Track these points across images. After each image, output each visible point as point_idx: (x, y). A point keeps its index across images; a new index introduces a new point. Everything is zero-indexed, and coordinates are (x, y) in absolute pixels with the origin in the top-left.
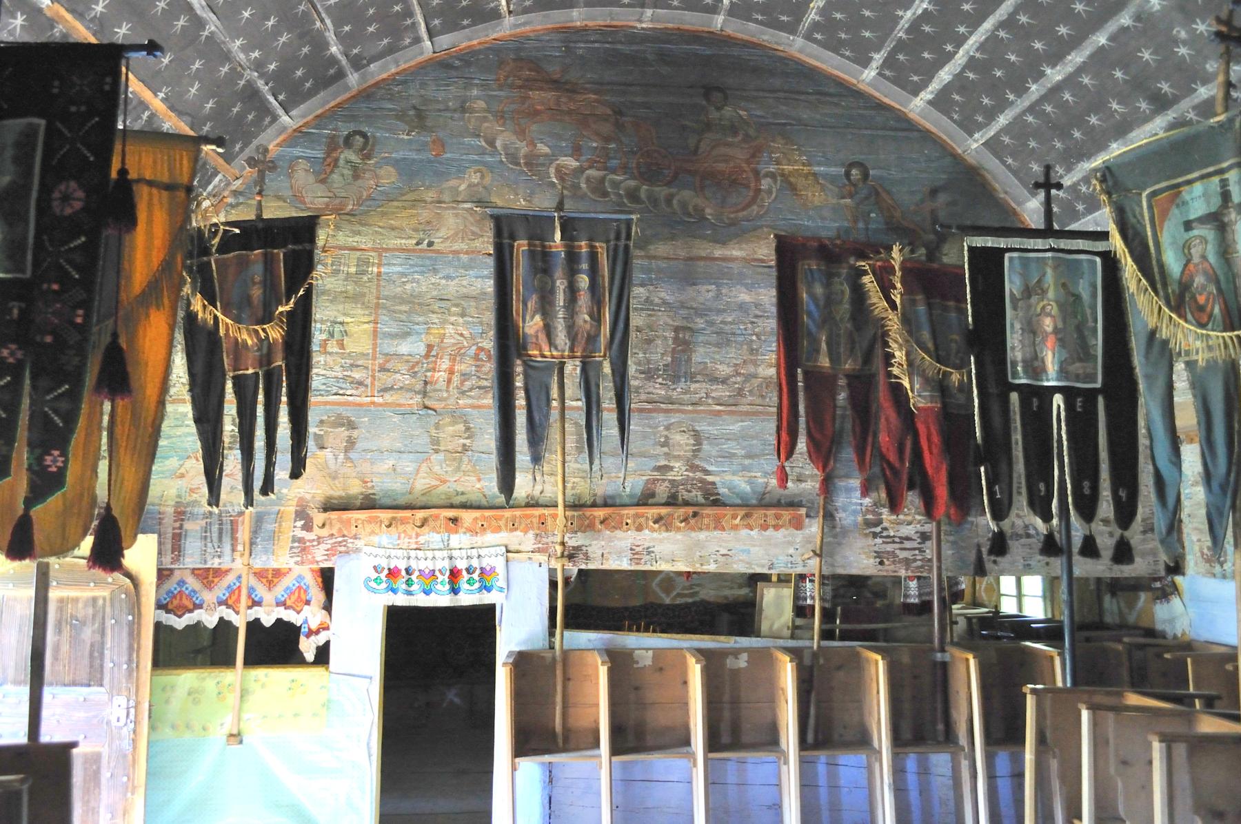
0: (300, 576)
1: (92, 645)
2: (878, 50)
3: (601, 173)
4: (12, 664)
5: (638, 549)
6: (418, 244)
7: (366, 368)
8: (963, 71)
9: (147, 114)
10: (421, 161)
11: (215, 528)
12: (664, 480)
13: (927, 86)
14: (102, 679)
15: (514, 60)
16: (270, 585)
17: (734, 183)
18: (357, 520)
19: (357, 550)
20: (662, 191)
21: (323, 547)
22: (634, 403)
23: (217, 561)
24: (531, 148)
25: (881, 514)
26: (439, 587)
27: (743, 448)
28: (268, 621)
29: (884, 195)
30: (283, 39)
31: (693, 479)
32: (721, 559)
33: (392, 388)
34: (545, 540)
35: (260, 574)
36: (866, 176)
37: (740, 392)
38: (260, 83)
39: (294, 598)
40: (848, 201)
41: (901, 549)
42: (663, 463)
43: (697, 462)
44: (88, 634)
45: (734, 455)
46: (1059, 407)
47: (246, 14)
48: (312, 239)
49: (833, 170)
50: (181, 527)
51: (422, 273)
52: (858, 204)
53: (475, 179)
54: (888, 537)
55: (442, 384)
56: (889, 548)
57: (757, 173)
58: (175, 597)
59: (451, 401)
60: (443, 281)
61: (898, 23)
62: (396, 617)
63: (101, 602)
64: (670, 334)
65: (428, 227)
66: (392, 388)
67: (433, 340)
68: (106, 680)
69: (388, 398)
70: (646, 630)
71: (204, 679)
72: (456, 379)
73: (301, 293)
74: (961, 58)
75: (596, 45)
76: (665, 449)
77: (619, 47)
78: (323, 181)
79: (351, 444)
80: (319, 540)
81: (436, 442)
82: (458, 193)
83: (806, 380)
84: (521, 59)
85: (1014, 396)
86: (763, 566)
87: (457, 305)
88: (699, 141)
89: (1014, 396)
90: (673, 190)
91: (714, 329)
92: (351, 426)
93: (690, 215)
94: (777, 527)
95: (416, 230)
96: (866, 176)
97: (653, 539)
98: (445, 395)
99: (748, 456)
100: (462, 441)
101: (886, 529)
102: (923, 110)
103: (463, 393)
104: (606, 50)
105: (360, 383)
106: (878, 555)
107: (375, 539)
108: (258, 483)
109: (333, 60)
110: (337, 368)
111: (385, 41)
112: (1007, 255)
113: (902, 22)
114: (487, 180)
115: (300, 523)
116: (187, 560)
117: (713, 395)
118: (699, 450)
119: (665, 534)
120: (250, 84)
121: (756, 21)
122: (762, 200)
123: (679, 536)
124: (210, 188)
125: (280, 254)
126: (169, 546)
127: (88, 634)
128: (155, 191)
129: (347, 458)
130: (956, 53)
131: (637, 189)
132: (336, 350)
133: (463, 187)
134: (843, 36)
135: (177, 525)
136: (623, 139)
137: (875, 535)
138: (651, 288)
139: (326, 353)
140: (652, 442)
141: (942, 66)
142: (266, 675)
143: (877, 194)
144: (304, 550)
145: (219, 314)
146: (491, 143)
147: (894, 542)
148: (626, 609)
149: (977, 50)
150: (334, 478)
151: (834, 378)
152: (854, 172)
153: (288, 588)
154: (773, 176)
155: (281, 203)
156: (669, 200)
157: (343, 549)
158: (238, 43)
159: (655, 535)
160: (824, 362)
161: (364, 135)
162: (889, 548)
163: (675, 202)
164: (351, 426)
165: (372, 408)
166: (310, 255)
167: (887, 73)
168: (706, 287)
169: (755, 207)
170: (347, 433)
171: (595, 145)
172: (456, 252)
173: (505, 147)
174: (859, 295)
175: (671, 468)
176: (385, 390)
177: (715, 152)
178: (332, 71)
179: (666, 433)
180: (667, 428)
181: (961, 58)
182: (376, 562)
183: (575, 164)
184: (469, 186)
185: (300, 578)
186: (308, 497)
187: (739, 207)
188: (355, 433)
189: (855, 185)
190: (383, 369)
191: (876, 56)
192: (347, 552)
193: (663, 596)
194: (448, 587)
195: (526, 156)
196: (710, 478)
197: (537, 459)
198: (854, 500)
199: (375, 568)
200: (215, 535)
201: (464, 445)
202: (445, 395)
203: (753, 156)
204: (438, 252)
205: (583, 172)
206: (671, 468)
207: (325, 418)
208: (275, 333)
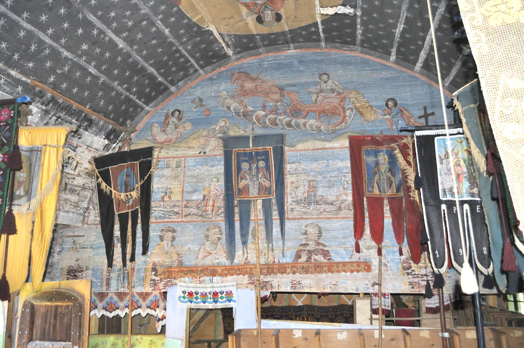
0: (155, 295)
1: (67, 325)
2: (392, 48)
3: (275, 116)
4: (39, 332)
5: (294, 282)
6: (200, 153)
7: (179, 207)
9: (83, 114)
10: (201, 119)
11: (122, 276)
12: (305, 250)
13: (418, 61)
14: (70, 339)
15: (238, 73)
16: (144, 299)
17: (334, 114)
18: (174, 271)
19: (176, 284)
20: (301, 121)
21: (162, 283)
22: (288, 214)
23: (122, 289)
24: (245, 108)
25: (410, 263)
26: (209, 300)
27: (341, 234)
28: (144, 314)
29: (405, 112)
30: (136, 79)
31: (318, 249)
32: (333, 286)
33: (190, 214)
34: (253, 279)
35: (140, 294)
36: (396, 104)
37: (340, 209)
38: (132, 96)
39: (154, 305)
40: (388, 116)
41: (422, 280)
42: (304, 242)
43: (320, 241)
44: (66, 320)
45: (338, 237)
47: (116, 72)
48: (151, 155)
49: (379, 104)
50: (109, 275)
51: (202, 165)
52: (393, 118)
53: (223, 124)
54: (415, 274)
55: (210, 212)
56: (416, 280)
57: (344, 109)
58: (109, 304)
59: (214, 219)
60: (210, 168)
61: (395, 35)
62: (192, 312)
63: (70, 307)
64: (307, 184)
65: (204, 146)
66: (190, 214)
67: (206, 193)
68: (71, 340)
69: (189, 218)
70: (296, 320)
71: (118, 339)
72: (215, 209)
73: (146, 178)
75: (272, 62)
76: (305, 236)
77: (281, 61)
78: (164, 131)
79: (174, 238)
80: (161, 280)
81: (207, 237)
82: (216, 131)
83: (368, 201)
84: (241, 72)
85: (444, 207)
86: (353, 290)
87: (216, 177)
88: (317, 97)
90: (307, 120)
91: (326, 180)
92: (174, 231)
93: (314, 131)
94: (358, 271)
95: (199, 147)
96: (396, 104)
97: (301, 278)
98: (211, 216)
99: (344, 237)
100: (218, 236)
101: (414, 271)
102: (420, 71)
103: (218, 215)
104: (276, 64)
105: (177, 213)
106: (410, 283)
107: (183, 279)
108: (128, 256)
109: (161, 84)
110: (168, 207)
111: (182, 73)
112: (436, 138)
113: (396, 34)
114: (227, 125)
115: (153, 273)
116: (112, 289)
117: (327, 210)
118: (320, 236)
119: (306, 275)
120: (126, 97)
121: (338, 42)
122: (347, 120)
123: (313, 276)
124: (120, 138)
125: (138, 163)
126: (105, 283)
127: (66, 320)
128: (52, 148)
129: (172, 245)
130: (424, 44)
131: (290, 121)
132: (168, 199)
133: (217, 128)
134: (375, 43)
135: (108, 274)
136: (284, 100)
137: (408, 274)
138: (298, 164)
139: (164, 201)
140: (299, 233)
141: (420, 51)
142: (141, 338)
143: (402, 111)
144: (155, 284)
145: (112, 189)
146: (229, 108)
147: (418, 277)
148: (330, 307)
150: (167, 254)
151: (382, 199)
152: (390, 103)
153: (151, 300)
154: (351, 109)
155: (148, 141)
156: (305, 125)
157: (170, 284)
158: (116, 83)
159: (302, 275)
160: (376, 191)
161: (179, 111)
162: (416, 280)
163: (307, 125)
164: (174, 231)
165: (182, 223)
166: (150, 162)
167: (400, 57)
168: (322, 162)
169: (344, 124)
170: (172, 234)
171: (272, 104)
172: (215, 155)
173: (234, 109)
174: (392, 159)
175: (308, 245)
176: (186, 216)
177: (324, 101)
178: (162, 88)
179: (305, 229)
180: (306, 227)
182: (183, 289)
183: (264, 113)
184: (220, 127)
185: (156, 296)
186: (157, 262)
187: (337, 124)
188: (175, 234)
189: (390, 109)
190: (186, 207)
192: (172, 285)
193: (348, 301)
194: (212, 300)
195: (243, 112)
196: (326, 249)
197: (244, 243)
198: (397, 257)
199: (183, 292)
200: (122, 278)
201: (219, 238)
202: (211, 216)
203: (342, 101)
204: (208, 156)
205: (267, 116)
206: (308, 245)
207: (164, 228)
208: (135, 194)
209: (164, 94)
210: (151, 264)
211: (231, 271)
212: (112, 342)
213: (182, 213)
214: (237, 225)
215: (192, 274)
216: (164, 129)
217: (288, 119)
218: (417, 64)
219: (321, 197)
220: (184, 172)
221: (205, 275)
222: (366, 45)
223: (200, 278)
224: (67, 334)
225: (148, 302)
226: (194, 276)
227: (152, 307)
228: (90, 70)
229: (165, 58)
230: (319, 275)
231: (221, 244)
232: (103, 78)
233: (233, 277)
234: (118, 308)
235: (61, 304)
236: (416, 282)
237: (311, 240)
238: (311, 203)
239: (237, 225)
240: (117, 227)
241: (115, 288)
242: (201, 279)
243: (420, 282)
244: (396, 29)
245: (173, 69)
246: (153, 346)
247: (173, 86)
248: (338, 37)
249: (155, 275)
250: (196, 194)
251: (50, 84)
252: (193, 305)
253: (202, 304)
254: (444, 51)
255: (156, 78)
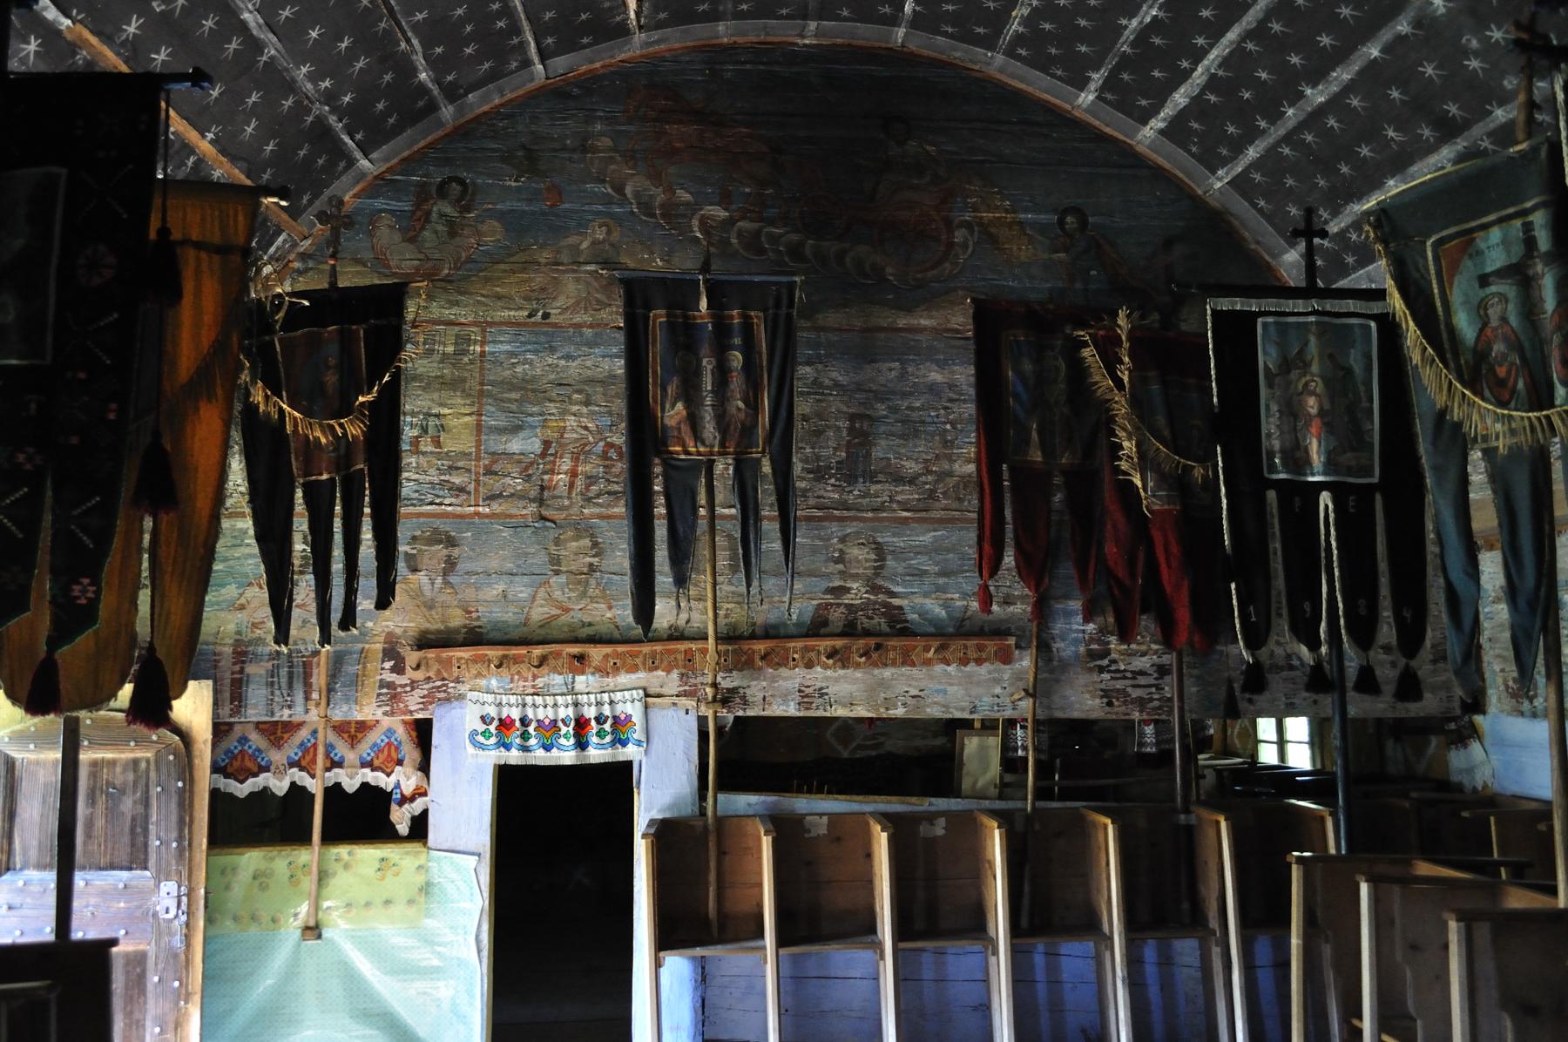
0: (389, 730)
1: (134, 819)
2: (1097, 70)
3: (756, 225)
4: (35, 843)
6: (530, 316)
7: (469, 471)
8: (1202, 92)
9: (192, 159)
10: (534, 213)
11: (284, 672)
12: (839, 605)
14: (146, 861)
16: (353, 741)
19: (461, 697)
21: (418, 693)
23: (286, 712)
26: (562, 741)
31: (875, 603)
33: (500, 495)
34: (692, 681)
35: (341, 728)
36: (1083, 224)
38: (332, 119)
39: (382, 757)
41: (1134, 686)
42: (837, 583)
43: (880, 582)
46: (1327, 507)
49: (1043, 217)
50: (242, 671)
53: (600, 234)
54: (1117, 671)
56: (1119, 685)
57: (948, 222)
59: (575, 510)
62: (507, 777)
63: (143, 765)
64: (844, 424)
66: (500, 495)
67: (551, 434)
68: (152, 862)
69: (496, 507)
71: (272, 859)
72: (580, 483)
74: (1199, 76)
76: (840, 567)
78: (412, 240)
79: (451, 564)
80: (414, 684)
81: (556, 561)
82: (579, 252)
85: (1272, 495)
86: (963, 710)
87: (579, 392)
89: (1272, 495)
92: (451, 542)
94: (979, 662)
96: (1083, 224)
97: (827, 678)
98: (567, 503)
100: (589, 559)
101: (1114, 661)
102: (1153, 141)
103: (589, 500)
105: (462, 490)
106: (1106, 694)
107: (483, 682)
110: (432, 471)
112: (1260, 320)
114: (615, 236)
115: (388, 665)
116: (250, 712)
118: (881, 567)
119: (841, 672)
121: (945, 34)
123: (858, 674)
124: (272, 250)
127: (128, 805)
128: (203, 255)
129: (446, 583)
130: (1194, 70)
132: (430, 448)
133: (585, 245)
135: (237, 668)
137: (1101, 670)
140: (823, 558)
142: (350, 854)
144: (395, 697)
146: (620, 190)
147: (1124, 678)
149: (1220, 66)
150: (431, 608)
152: (1069, 219)
153: (375, 745)
154: (968, 225)
157: (442, 695)
158: (304, 70)
159: (829, 672)
160: (1037, 456)
161: (461, 182)
162: (1119, 685)
163: (848, 260)
164: (451, 542)
165: (477, 520)
167: (1109, 96)
169: (947, 265)
172: (578, 326)
173: (637, 194)
176: (492, 498)
181: (1199, 76)
183: (724, 214)
184: (593, 243)
186: (399, 631)
188: (456, 552)
190: (489, 472)
191: (1095, 76)
192: (448, 700)
194: (572, 741)
195: (662, 206)
196: (896, 602)
197: (681, 581)
200: (284, 680)
201: (591, 565)
202: (567, 503)
204: (555, 325)
206: (848, 590)
207: (418, 533)
208: (355, 429)
209: (420, 126)
210: (382, 639)
211: (629, 661)
212: (251, 870)
213: (476, 490)
214: (661, 531)
215: (514, 669)
216: (412, 233)
217: (795, 237)
218: (1153, 123)
219: (884, 463)
220: (482, 369)
221: (555, 670)
222: (1024, 53)
223: (535, 677)
224: (133, 845)
225: (291, 750)
226: (519, 673)
227: (376, 763)
228: (246, 16)
229: (460, 11)
230: (876, 671)
231: (598, 584)
232: (273, 48)
233: (633, 676)
234: (267, 769)
235: (109, 755)
236: (1118, 690)
237: (855, 577)
238: (856, 477)
239: (661, 531)
240: (301, 524)
241: (262, 709)
242: (540, 682)
243: (1129, 690)
244: (1132, 17)
245: (468, 51)
246: (389, 873)
247: (451, 102)
248: (955, 19)
249: (393, 670)
250: (522, 434)
251: (123, 44)
252: (514, 757)
253: (540, 753)
254: (1247, 95)
255: (414, 71)
